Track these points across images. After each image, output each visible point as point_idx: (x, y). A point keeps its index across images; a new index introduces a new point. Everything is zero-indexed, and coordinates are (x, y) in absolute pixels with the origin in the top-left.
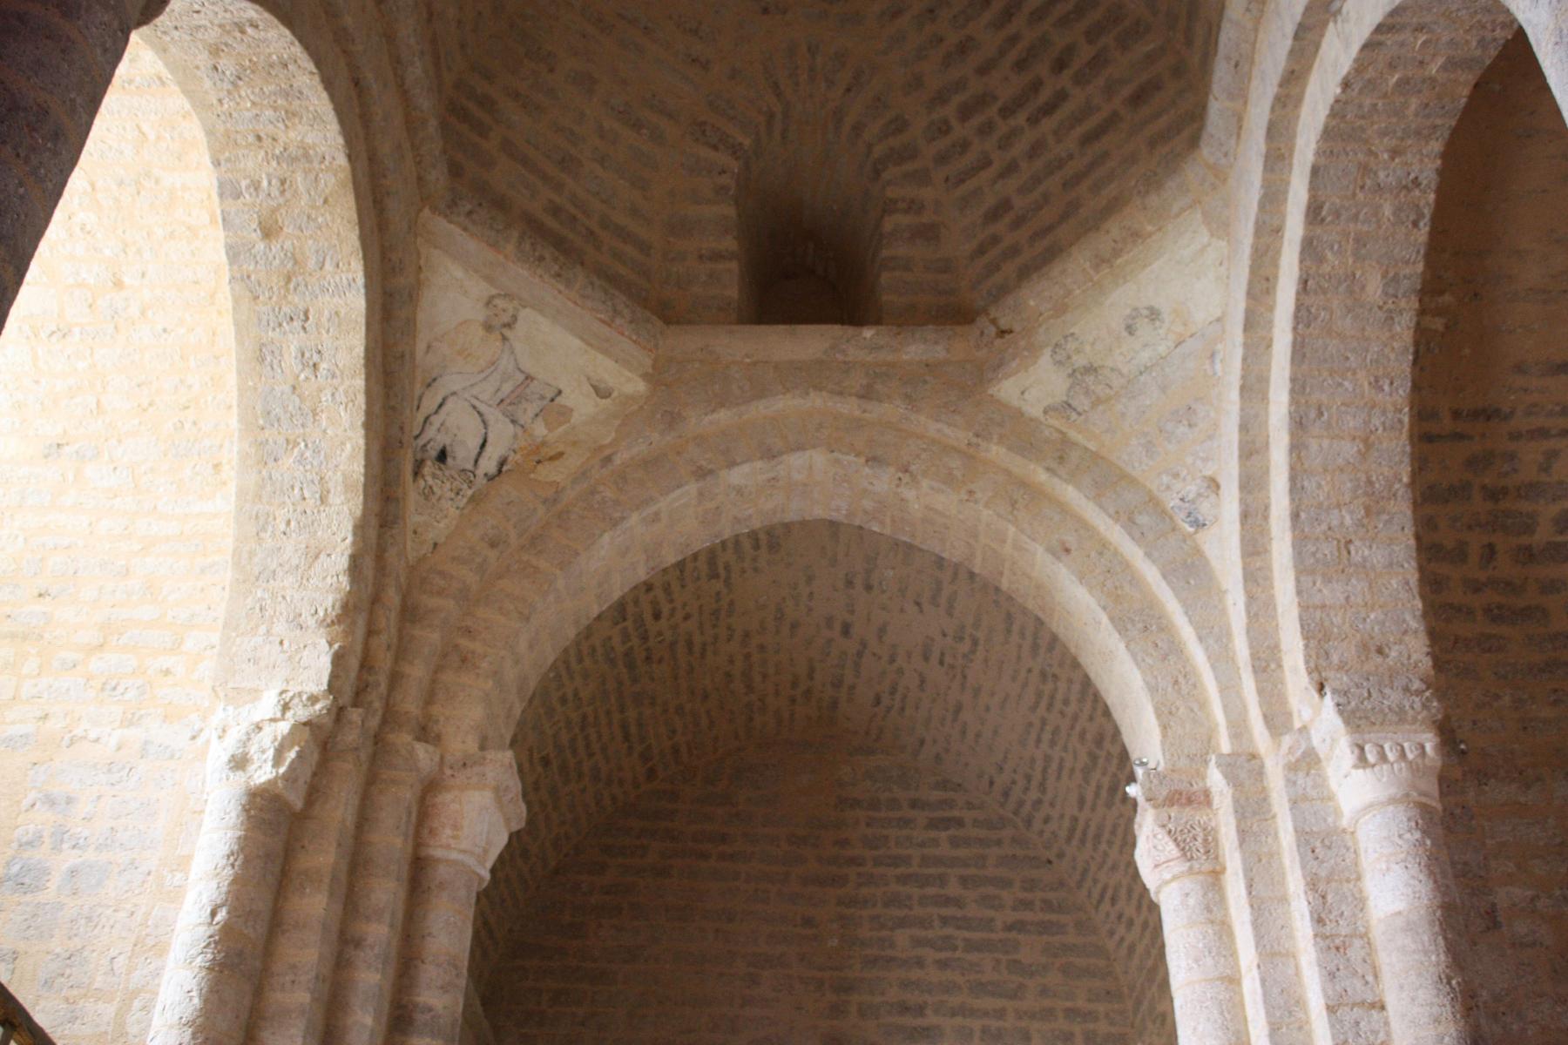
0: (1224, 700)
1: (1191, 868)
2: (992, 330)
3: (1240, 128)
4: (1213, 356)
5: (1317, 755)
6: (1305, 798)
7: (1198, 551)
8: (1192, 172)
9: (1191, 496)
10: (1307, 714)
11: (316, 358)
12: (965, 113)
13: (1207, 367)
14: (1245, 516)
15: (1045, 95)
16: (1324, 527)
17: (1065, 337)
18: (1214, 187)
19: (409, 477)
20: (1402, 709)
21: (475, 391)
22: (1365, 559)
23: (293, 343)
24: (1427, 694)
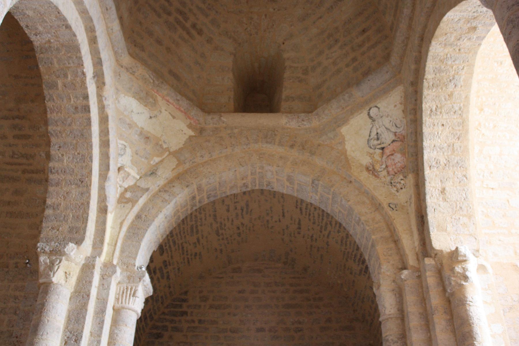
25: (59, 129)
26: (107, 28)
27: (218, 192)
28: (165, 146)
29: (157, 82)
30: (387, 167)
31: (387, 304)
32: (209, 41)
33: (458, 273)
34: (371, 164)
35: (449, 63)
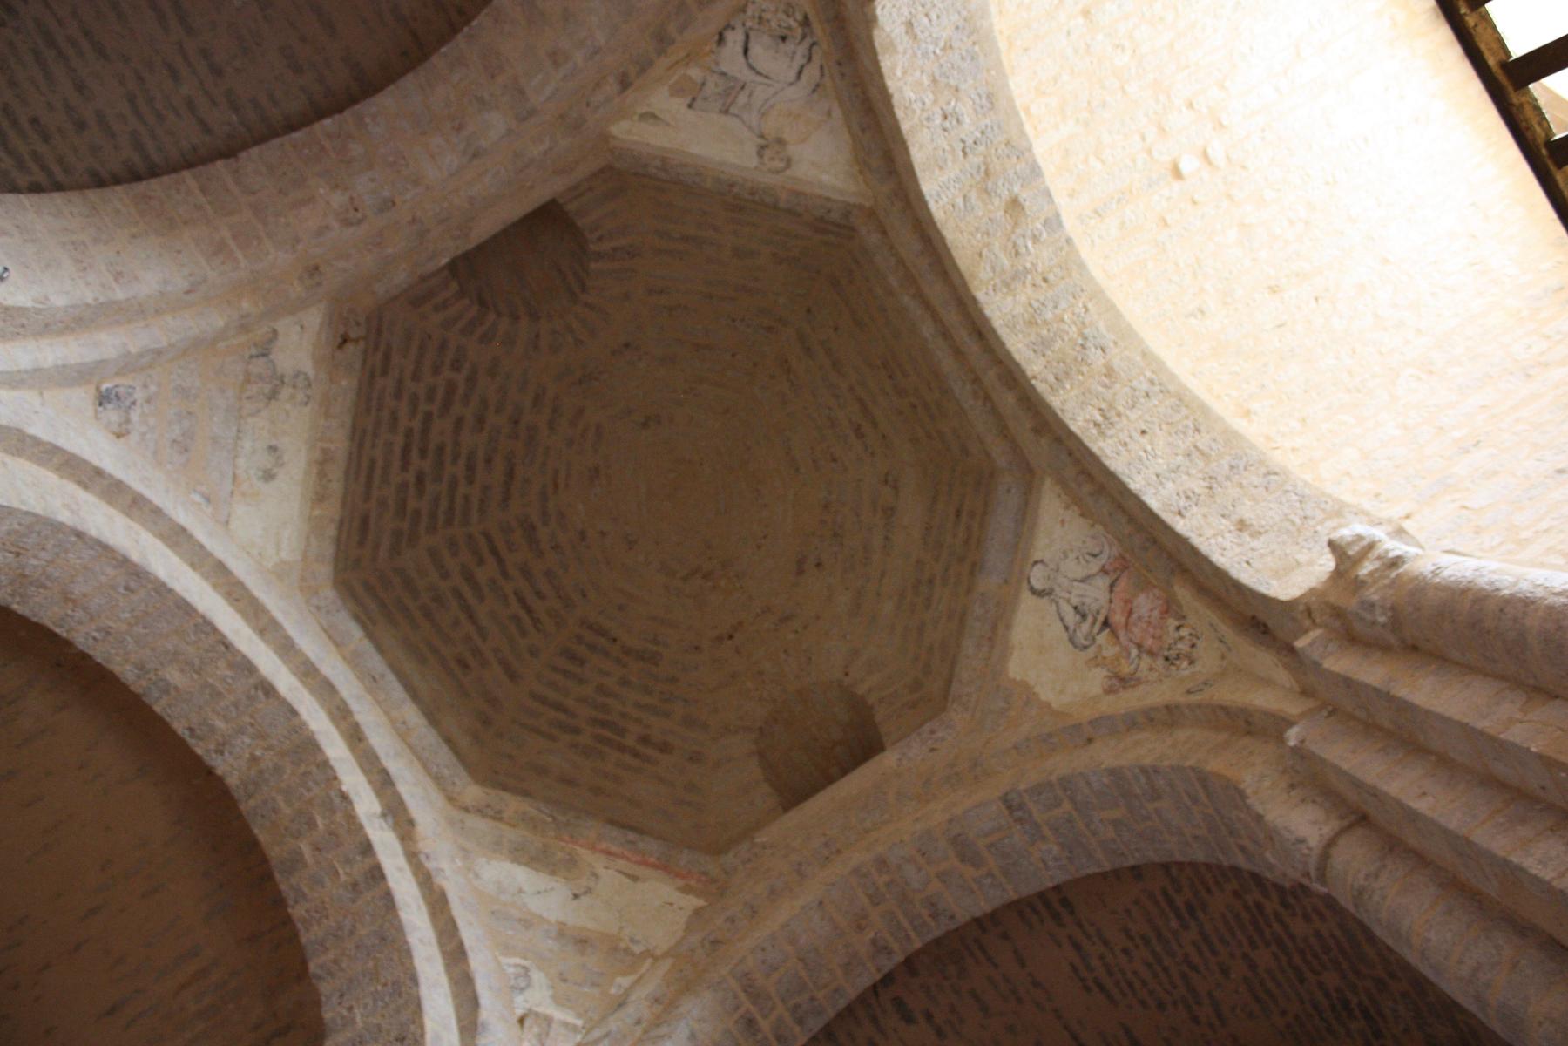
2: (353, 335)
3: (330, 637)
4: (208, 499)
8: (325, 571)
11: (947, 124)
12: (451, 388)
14: (99, 472)
15: (415, 454)
17: (309, 397)
18: (303, 579)
19: (812, 18)
21: (771, 91)
23: (969, 127)
25: (331, 956)
26: (393, 722)
27: (820, 995)
28: (637, 949)
29: (561, 818)
30: (1139, 646)
31: (1302, 824)
32: (695, 758)
33: (1371, 574)
34: (1110, 678)
35: (1049, 316)
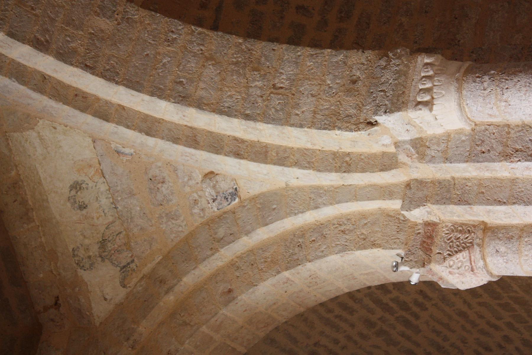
0: (366, 198)
1: (479, 245)
2: (52, 311)
4: (118, 152)
5: (417, 139)
6: (445, 152)
7: (254, 199)
9: (214, 193)
10: (386, 140)
13: (125, 159)
14: (238, 155)
16: (259, 100)
17: (74, 255)
20: (397, 72)
22: (288, 79)
24: (391, 55)
